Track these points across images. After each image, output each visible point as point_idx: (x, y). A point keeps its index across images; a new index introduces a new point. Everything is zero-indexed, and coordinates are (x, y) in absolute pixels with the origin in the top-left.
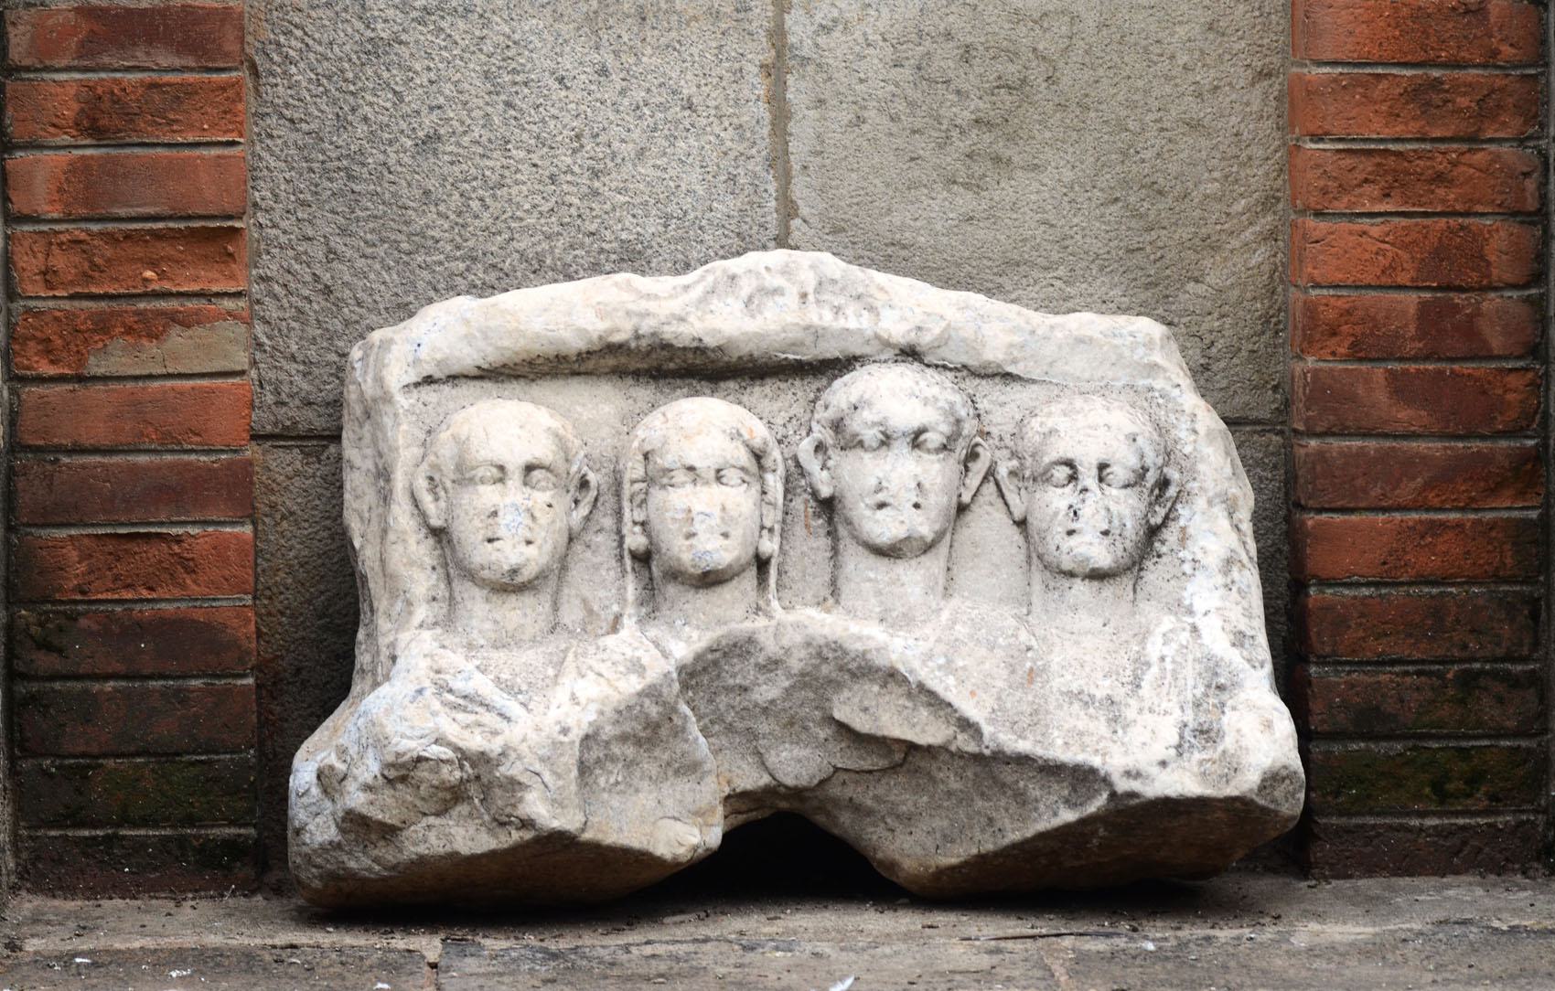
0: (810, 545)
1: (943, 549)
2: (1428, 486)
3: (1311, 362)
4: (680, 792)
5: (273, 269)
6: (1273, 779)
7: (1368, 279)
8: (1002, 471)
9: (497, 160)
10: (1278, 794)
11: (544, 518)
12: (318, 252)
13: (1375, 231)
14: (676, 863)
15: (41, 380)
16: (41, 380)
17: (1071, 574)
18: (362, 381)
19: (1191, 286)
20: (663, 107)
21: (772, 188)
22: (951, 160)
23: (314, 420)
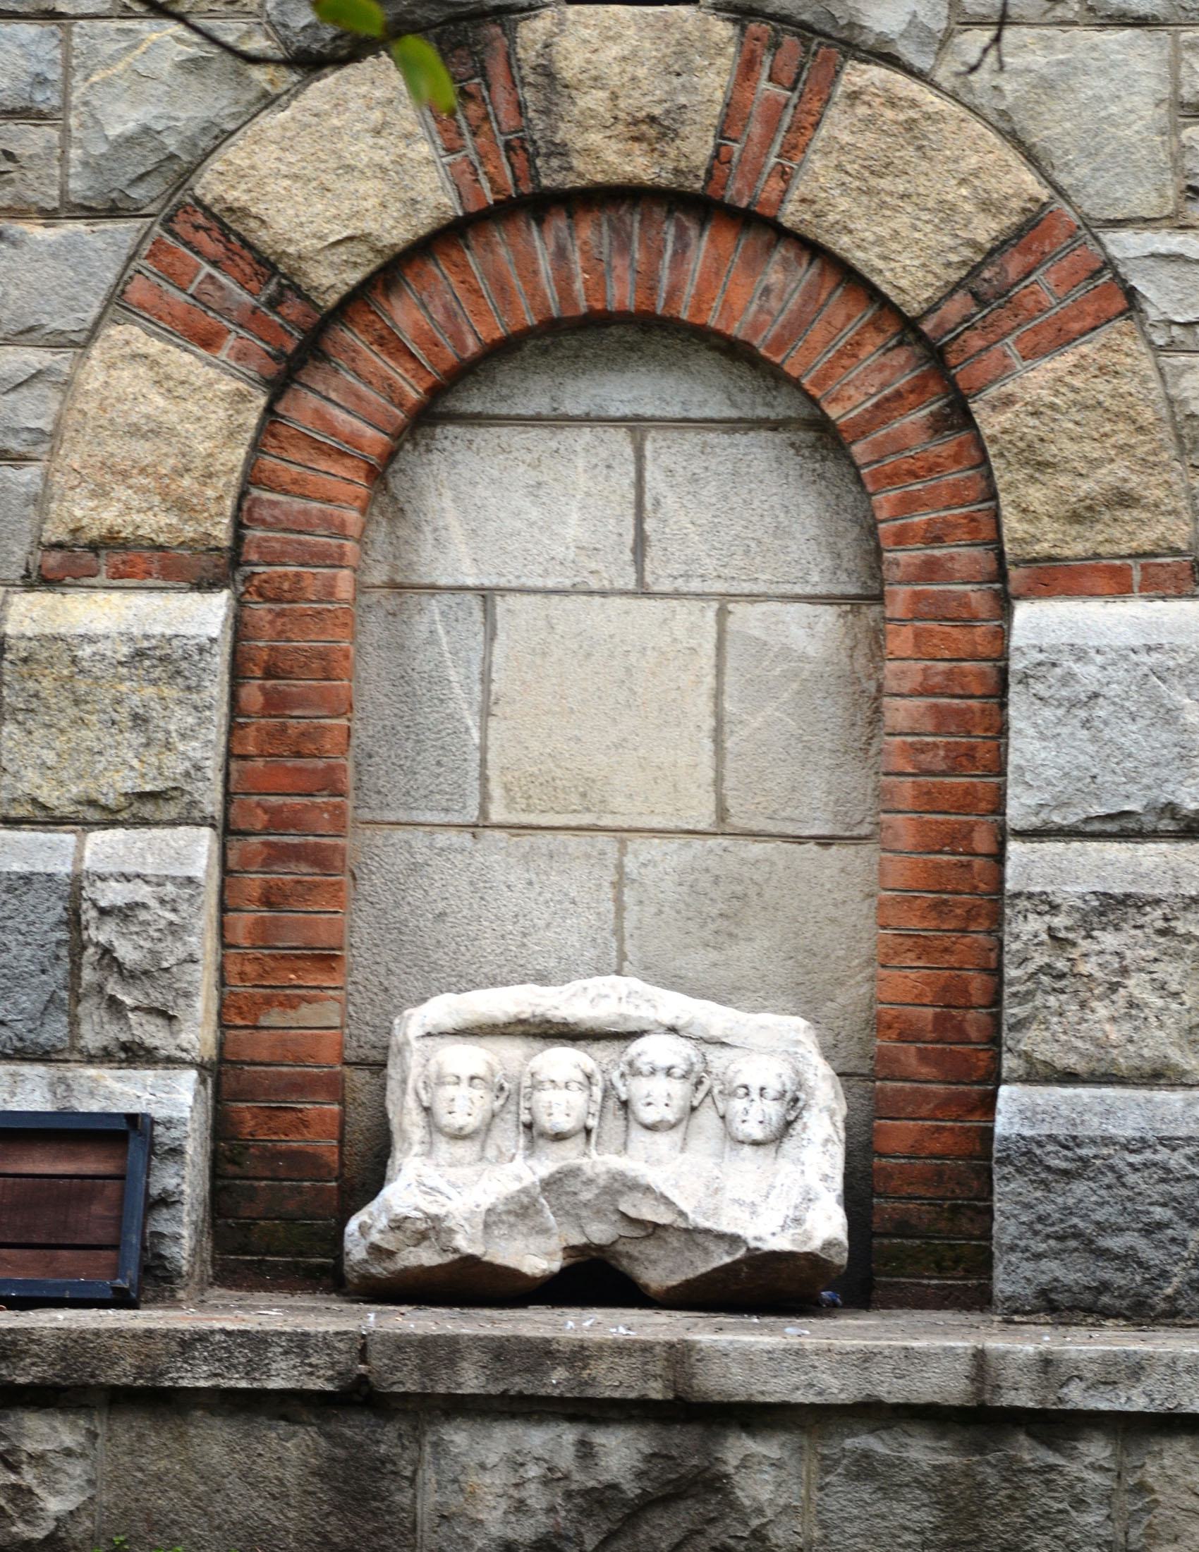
0: (614, 1123)
1: (682, 1128)
2: (936, 1107)
3: (878, 1042)
4: (537, 1242)
5: (358, 977)
6: (829, 1244)
7: (908, 1000)
8: (716, 1091)
9: (474, 927)
10: (833, 1252)
11: (478, 1103)
12: (382, 970)
13: (913, 976)
14: (534, 1279)
15: (236, 1027)
16: (236, 1027)
17: (743, 1142)
18: (398, 1035)
19: (829, 1004)
20: (560, 902)
21: (615, 945)
22: (707, 934)
23: (375, 1055)
